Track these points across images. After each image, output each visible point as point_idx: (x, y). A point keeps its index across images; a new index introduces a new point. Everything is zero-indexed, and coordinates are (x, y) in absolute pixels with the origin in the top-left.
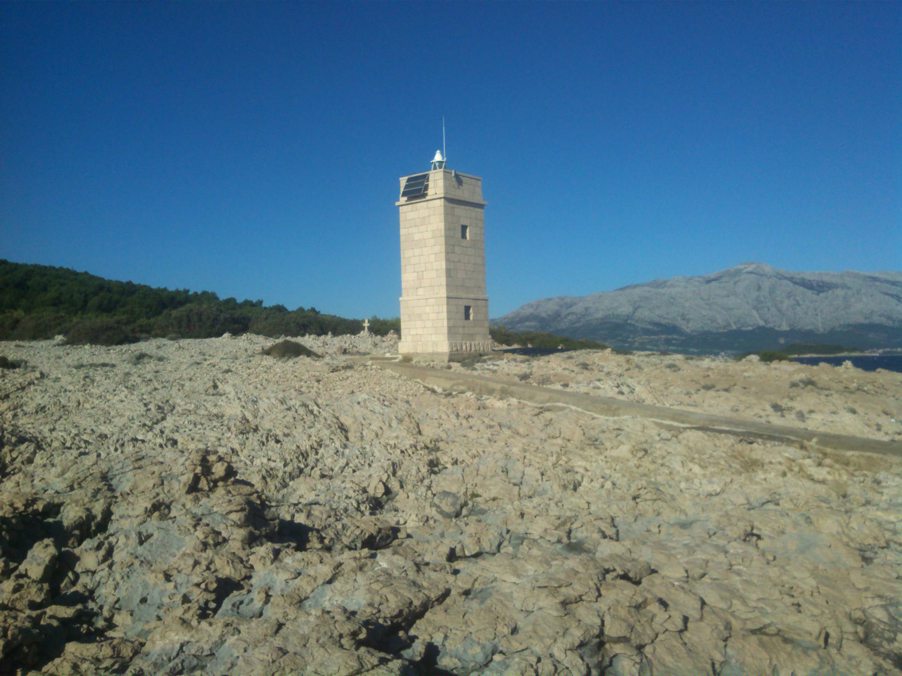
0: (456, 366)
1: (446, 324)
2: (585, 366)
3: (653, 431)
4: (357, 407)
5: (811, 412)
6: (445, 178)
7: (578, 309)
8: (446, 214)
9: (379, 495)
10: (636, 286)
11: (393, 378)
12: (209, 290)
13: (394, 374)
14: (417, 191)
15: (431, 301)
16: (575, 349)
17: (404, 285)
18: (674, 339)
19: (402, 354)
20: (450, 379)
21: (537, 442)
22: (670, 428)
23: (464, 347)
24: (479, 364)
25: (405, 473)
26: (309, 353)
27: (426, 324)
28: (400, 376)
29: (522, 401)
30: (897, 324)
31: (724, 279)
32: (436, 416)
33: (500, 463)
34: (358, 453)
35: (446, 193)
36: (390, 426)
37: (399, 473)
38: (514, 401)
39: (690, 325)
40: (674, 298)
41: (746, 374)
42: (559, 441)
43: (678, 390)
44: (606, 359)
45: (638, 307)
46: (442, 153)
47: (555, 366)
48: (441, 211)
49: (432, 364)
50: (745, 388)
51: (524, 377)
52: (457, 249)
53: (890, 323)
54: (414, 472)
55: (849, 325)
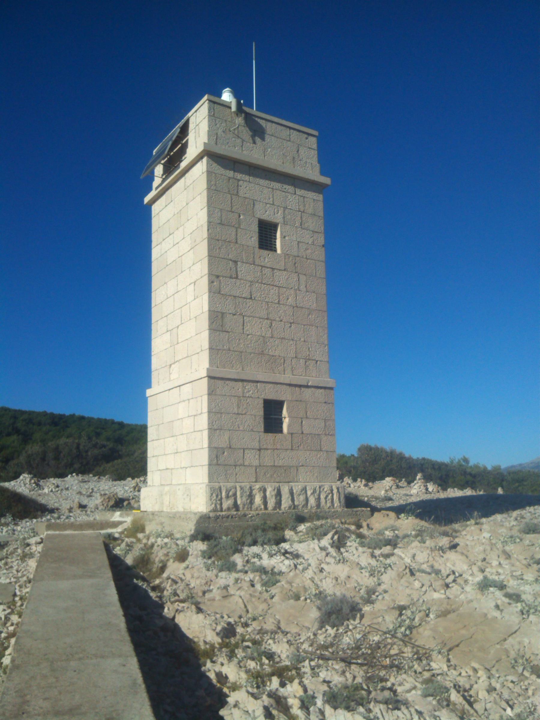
23: (258, 500)
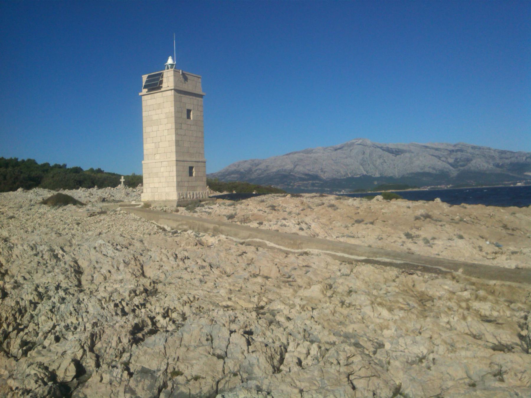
0: (182, 209)
1: (175, 180)
2: (273, 208)
3: (335, 266)
4: (93, 251)
5: (434, 239)
6: (175, 76)
7: (262, 166)
8: (175, 101)
9: (69, 379)
10: (295, 153)
11: (135, 220)
12: (32, 158)
13: (136, 217)
14: (155, 85)
15: (165, 164)
16: (264, 194)
17: (145, 152)
18: (316, 183)
19: (144, 202)
20: (177, 221)
21: (241, 281)
22: (343, 261)
23: (188, 196)
24: (199, 208)
25: (105, 345)
26: (75, 202)
27: (161, 182)
28: (141, 218)
29: (229, 237)
30: (438, 172)
31: (345, 148)
32: (158, 259)
33: (206, 330)
34: (72, 309)
35: (175, 86)
36: (118, 269)
37: (98, 345)
38: (223, 237)
39: (325, 175)
40: (317, 160)
41: (383, 211)
42: (259, 280)
43: (339, 224)
44: (288, 203)
45: (297, 165)
46: (173, 59)
47: (252, 208)
48: (172, 98)
49: (165, 208)
50: (384, 221)
51: (231, 217)
52: (183, 126)
53: (434, 172)
54: (114, 344)
55: (412, 173)
